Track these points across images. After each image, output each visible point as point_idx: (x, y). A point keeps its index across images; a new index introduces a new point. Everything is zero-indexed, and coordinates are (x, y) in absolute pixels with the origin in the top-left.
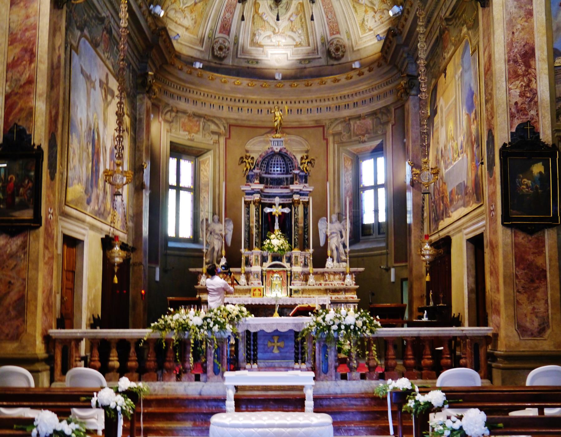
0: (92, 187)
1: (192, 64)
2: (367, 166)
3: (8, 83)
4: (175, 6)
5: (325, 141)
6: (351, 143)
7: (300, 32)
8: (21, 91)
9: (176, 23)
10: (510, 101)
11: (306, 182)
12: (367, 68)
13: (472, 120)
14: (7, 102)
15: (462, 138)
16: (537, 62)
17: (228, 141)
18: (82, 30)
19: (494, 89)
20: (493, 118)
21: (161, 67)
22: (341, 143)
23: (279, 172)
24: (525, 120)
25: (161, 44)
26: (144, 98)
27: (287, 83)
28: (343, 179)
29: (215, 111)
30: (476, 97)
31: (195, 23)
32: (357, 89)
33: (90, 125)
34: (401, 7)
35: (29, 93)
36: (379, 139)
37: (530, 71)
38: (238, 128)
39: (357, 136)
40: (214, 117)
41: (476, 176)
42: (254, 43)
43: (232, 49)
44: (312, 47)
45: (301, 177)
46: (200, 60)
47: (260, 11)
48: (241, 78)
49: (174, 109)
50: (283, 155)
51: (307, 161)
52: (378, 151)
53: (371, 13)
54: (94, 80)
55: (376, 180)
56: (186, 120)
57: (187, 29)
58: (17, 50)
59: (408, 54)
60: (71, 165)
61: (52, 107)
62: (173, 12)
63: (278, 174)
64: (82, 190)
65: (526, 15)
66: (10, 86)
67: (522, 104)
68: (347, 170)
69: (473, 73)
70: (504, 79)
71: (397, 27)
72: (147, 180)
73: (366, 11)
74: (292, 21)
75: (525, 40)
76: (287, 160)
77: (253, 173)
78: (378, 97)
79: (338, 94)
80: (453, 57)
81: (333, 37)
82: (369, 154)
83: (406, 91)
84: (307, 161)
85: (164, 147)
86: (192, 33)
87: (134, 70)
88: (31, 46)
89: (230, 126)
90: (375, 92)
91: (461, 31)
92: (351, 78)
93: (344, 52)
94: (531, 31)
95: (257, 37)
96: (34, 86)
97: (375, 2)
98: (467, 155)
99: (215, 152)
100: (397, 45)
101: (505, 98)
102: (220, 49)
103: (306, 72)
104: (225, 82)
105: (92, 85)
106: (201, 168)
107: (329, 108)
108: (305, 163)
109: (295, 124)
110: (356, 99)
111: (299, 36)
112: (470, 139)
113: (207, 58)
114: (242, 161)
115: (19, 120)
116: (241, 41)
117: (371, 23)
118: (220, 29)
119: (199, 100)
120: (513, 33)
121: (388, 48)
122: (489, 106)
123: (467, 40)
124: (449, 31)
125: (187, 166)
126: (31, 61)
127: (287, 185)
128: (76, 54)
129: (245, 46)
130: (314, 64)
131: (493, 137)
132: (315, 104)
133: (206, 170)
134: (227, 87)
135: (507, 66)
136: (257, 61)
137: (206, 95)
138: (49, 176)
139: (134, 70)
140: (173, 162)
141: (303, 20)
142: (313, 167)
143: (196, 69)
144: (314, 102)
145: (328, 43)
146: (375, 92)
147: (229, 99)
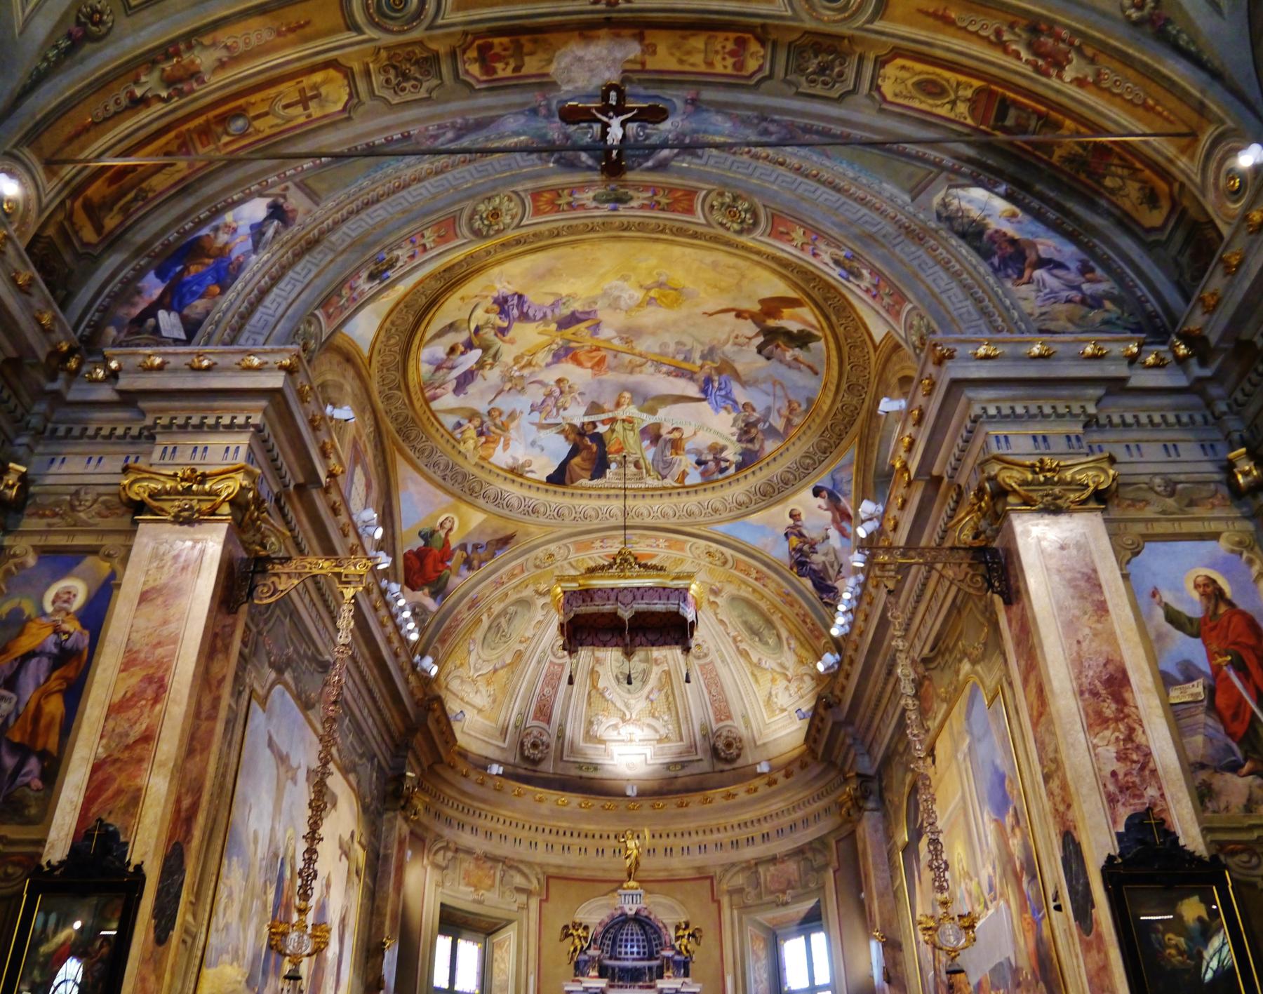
0: (265, 973)
1: (486, 769)
2: (793, 949)
3: (104, 741)
4: (462, 672)
5: (715, 905)
6: (762, 906)
7: (666, 718)
8: (126, 755)
9: (462, 699)
10: (1100, 769)
11: (686, 975)
12: (783, 772)
13: (1009, 829)
14: (95, 777)
15: (990, 870)
16: (1137, 695)
17: (544, 905)
18: (280, 671)
19: (1062, 748)
20: (1069, 806)
21: (430, 767)
22: (745, 908)
23: (635, 956)
24: (1140, 808)
25: (431, 725)
26: (395, 817)
27: (647, 803)
28: (751, 976)
29: (523, 852)
30: (1011, 781)
31: (494, 701)
32: (766, 811)
33: (277, 849)
34: (837, 656)
35: (140, 760)
36: (811, 898)
37: (1126, 710)
38: (564, 882)
39: (772, 893)
40: (522, 862)
41: (1039, 941)
42: (590, 737)
43: (553, 745)
44: (686, 742)
45: (677, 964)
46: (500, 763)
47: (600, 685)
48: (568, 794)
49: (452, 845)
50: (642, 921)
51: (687, 933)
52: (811, 921)
53: (782, 683)
54: (295, 765)
55: (812, 978)
56: (472, 866)
57: (480, 711)
58: (134, 681)
59: (855, 739)
60: (219, 921)
61: (183, 790)
62: (458, 681)
63: (634, 960)
64: (239, 978)
65: (1096, 611)
66: (106, 747)
67: (1126, 775)
68: (758, 960)
69: (996, 738)
70: (1079, 727)
71: (832, 693)
72: (390, 973)
73: (773, 680)
74: (652, 701)
75: (1105, 655)
76: (650, 931)
77: (586, 958)
78: (806, 822)
79: (734, 820)
80: (947, 724)
81: (721, 724)
82: (795, 928)
83: (858, 804)
84: (687, 933)
85: (429, 914)
86: (488, 718)
87: (380, 767)
88: (160, 674)
89: (548, 878)
90: (799, 814)
91: (957, 672)
92: (756, 790)
93: (740, 749)
94: (1112, 638)
95: (595, 727)
96: (152, 745)
97: (787, 664)
98: (1007, 902)
99: (520, 925)
100: (835, 724)
101: (1089, 764)
102: (535, 745)
103: (678, 784)
104: (541, 800)
105: (290, 774)
106: (496, 956)
107: (719, 846)
108: (683, 937)
109: (662, 875)
110: (766, 827)
111: (665, 726)
112: (1009, 868)
113: (511, 760)
114: (566, 934)
115: (110, 813)
116: (568, 733)
117: (782, 699)
118: (535, 713)
119: (496, 830)
120: (1079, 642)
121: (819, 731)
122: (1055, 784)
123: (975, 684)
124: (930, 679)
125: (469, 952)
126: (156, 700)
127: (651, 980)
128: (260, 710)
129: (576, 741)
130: (688, 771)
131: (1078, 847)
132: (695, 838)
133: (503, 960)
134: (544, 809)
135: (1080, 704)
136: (596, 767)
137: (508, 823)
138: (152, 935)
139: (380, 767)
140: (443, 944)
141: (671, 699)
142: (699, 944)
143: (491, 776)
144: (693, 835)
145: (714, 734)
146: (799, 814)
147: (547, 831)
